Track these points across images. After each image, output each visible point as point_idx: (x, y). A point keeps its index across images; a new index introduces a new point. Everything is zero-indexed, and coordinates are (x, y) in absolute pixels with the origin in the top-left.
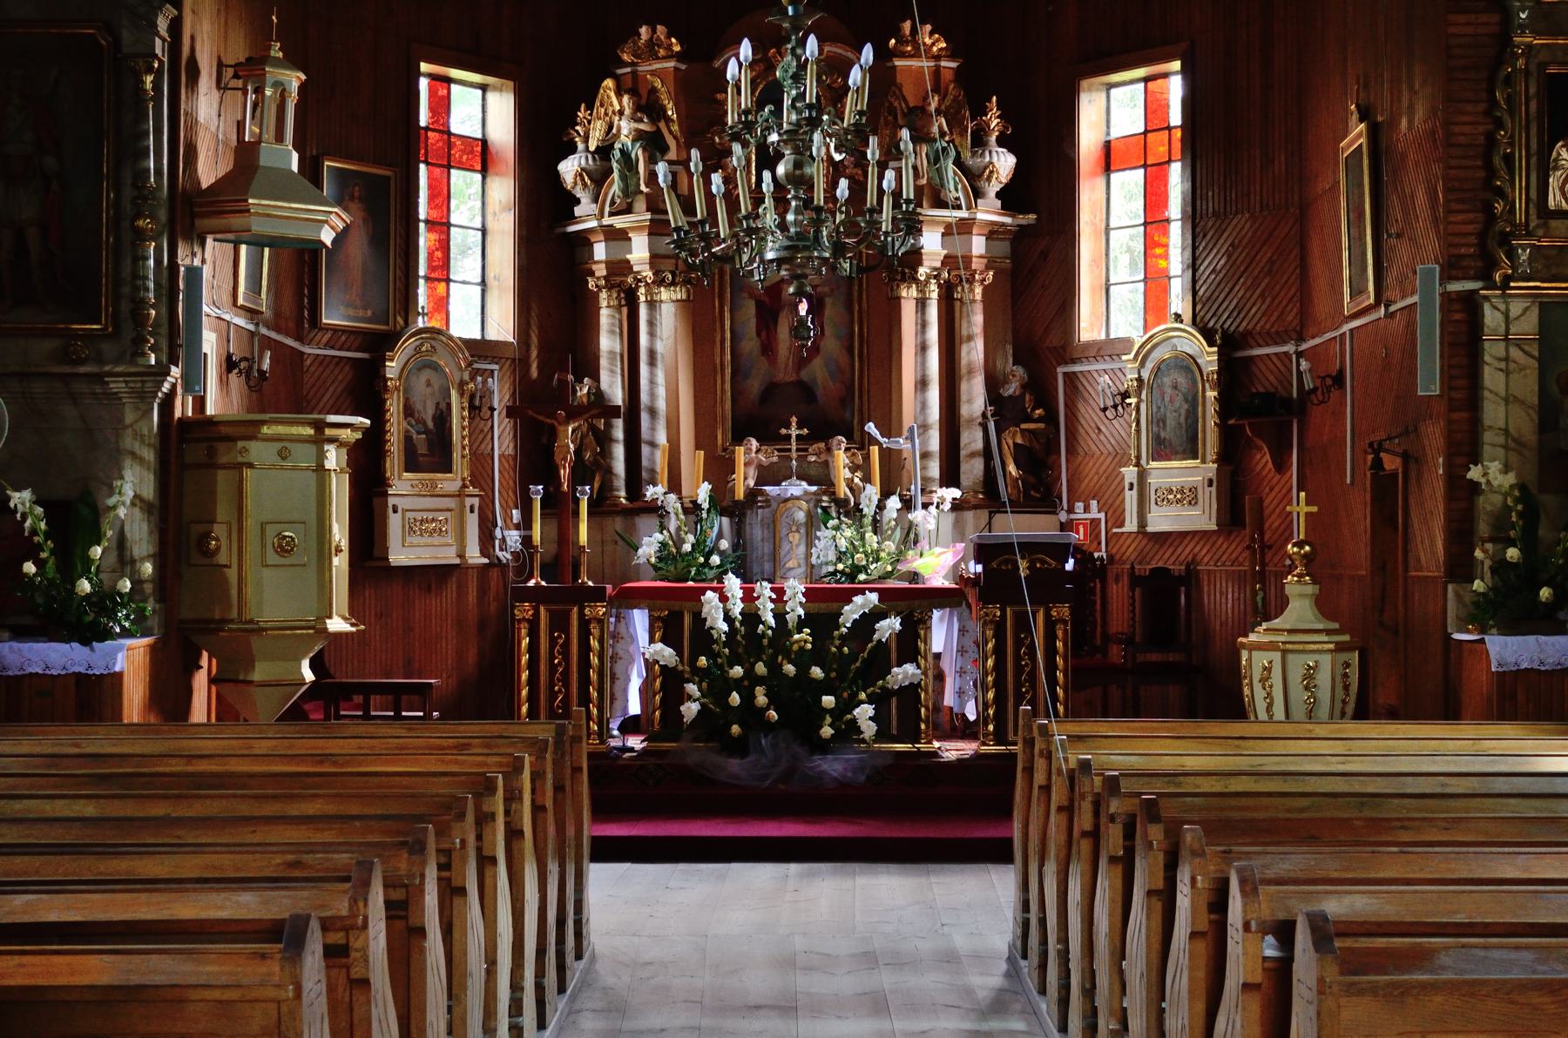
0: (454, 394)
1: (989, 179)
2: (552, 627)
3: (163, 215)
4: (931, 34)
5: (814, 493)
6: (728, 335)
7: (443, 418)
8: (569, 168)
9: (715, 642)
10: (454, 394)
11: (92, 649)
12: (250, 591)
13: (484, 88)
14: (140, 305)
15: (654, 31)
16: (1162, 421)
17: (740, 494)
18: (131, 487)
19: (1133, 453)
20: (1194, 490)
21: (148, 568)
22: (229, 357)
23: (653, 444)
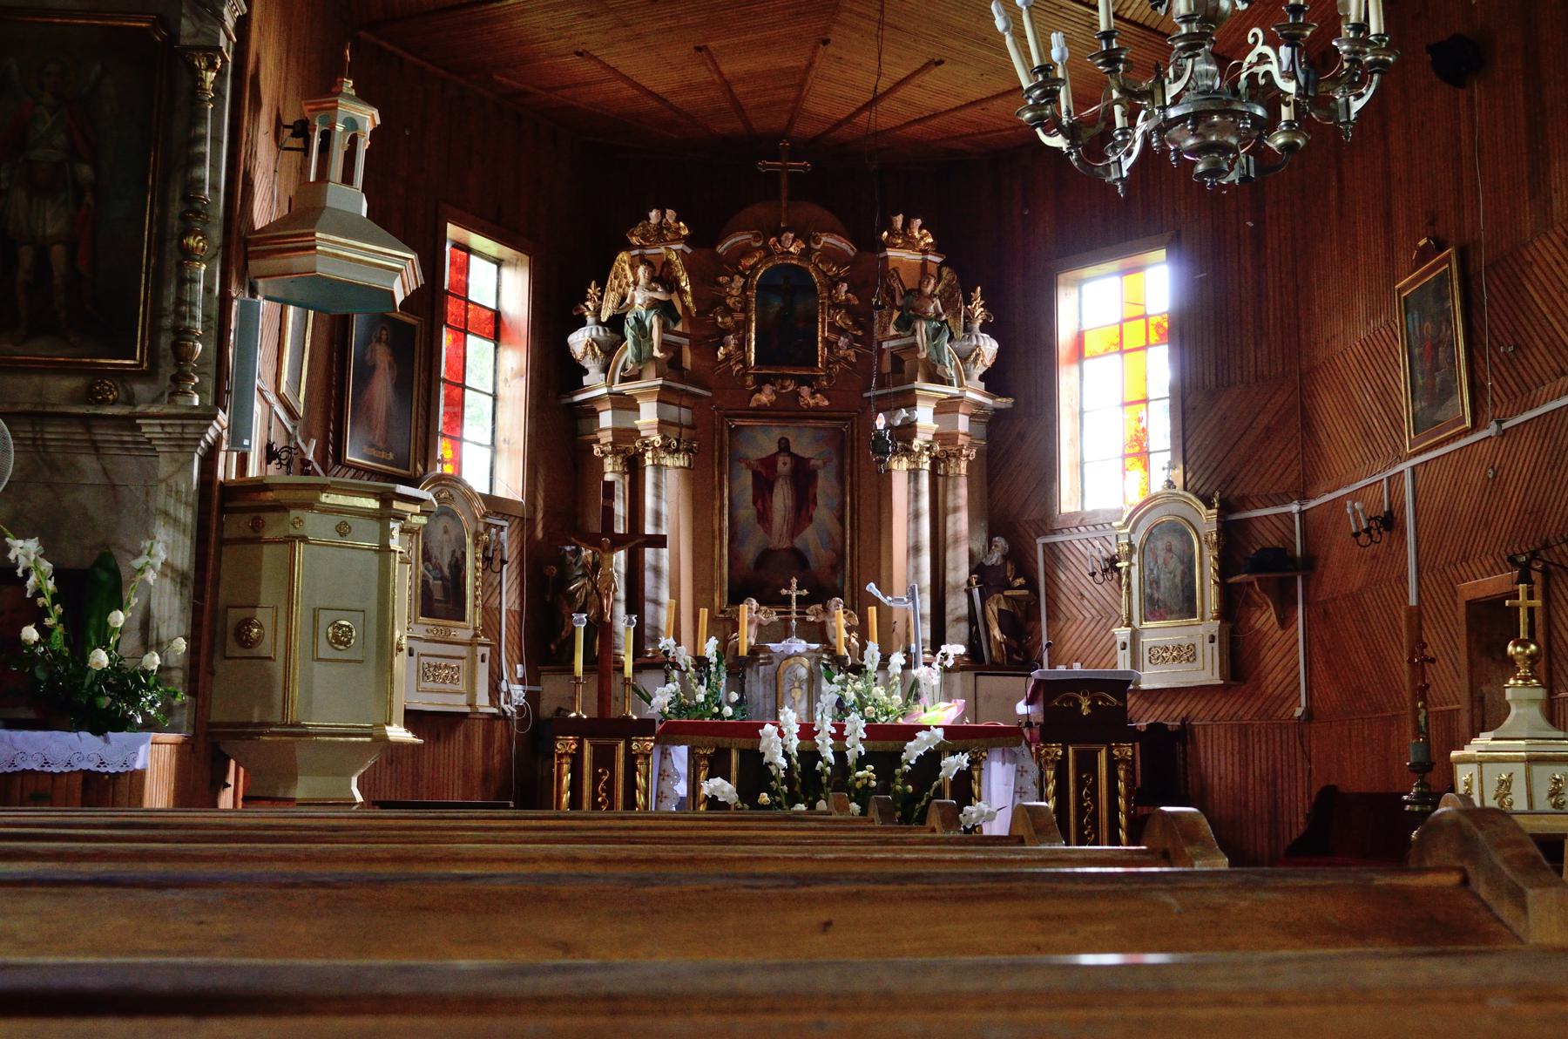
0: (469, 541)
1: (975, 361)
2: (596, 763)
3: (216, 235)
4: (921, 228)
5: (815, 651)
6: (726, 502)
7: (458, 566)
8: (578, 340)
9: (774, 778)
10: (469, 541)
11: (107, 741)
12: (297, 691)
13: (499, 262)
14: (182, 334)
15: (663, 215)
16: (1155, 583)
17: (743, 651)
18: (160, 555)
19: (1124, 613)
20: (1192, 647)
21: (181, 645)
22: (269, 446)
23: (657, 603)
